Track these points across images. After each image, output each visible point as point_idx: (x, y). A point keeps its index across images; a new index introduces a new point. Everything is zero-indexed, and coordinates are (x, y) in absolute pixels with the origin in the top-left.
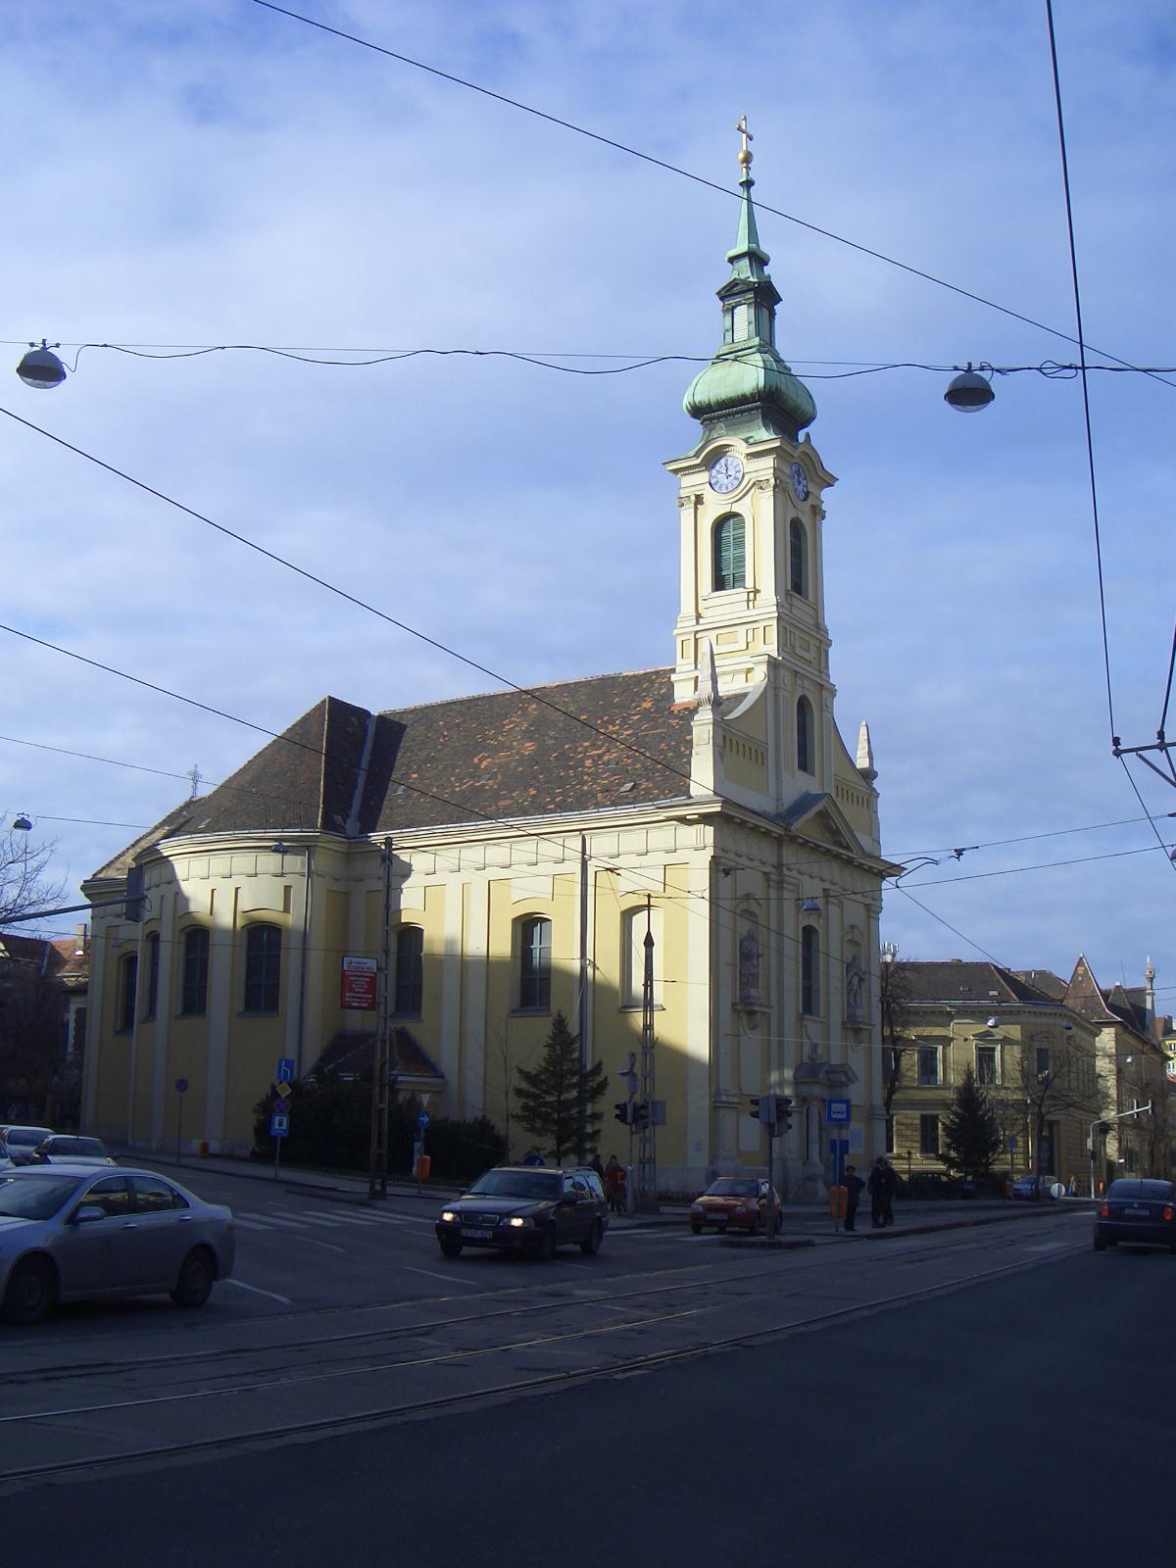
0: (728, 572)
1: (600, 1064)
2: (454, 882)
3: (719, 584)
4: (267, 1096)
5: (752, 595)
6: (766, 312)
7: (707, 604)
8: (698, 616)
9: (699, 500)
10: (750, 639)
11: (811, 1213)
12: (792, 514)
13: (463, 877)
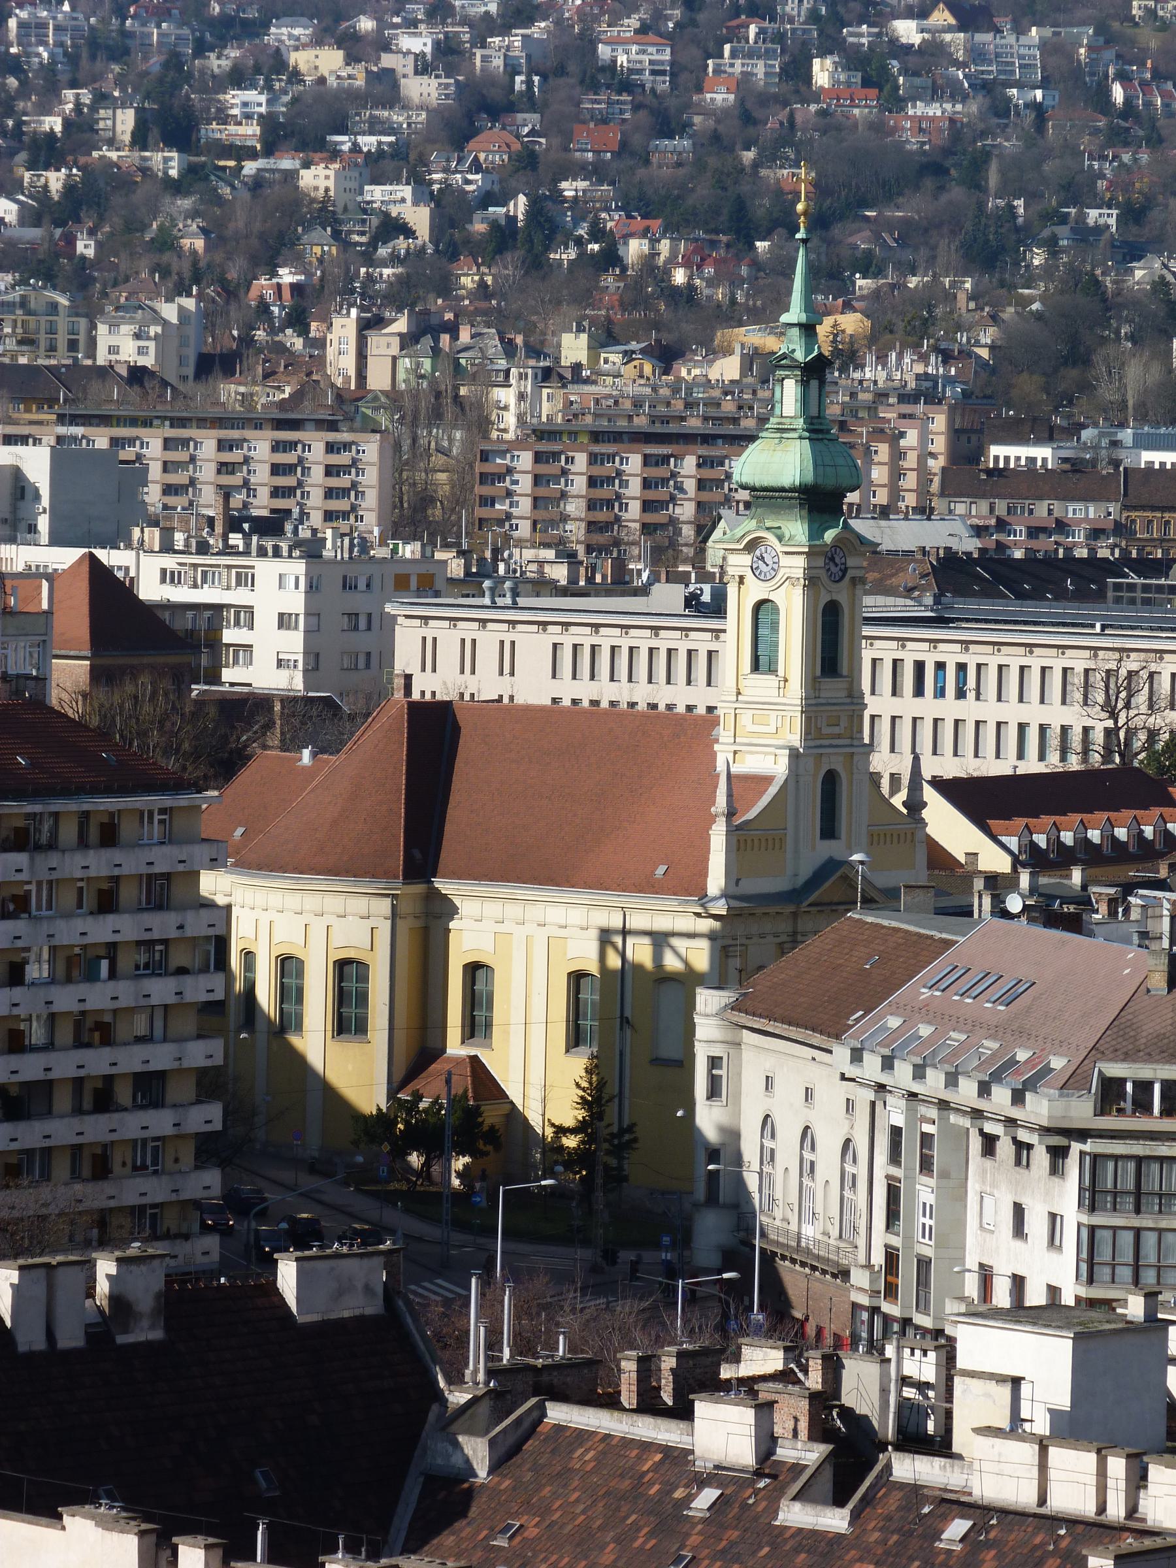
0: (763, 660)
1: (634, 1125)
2: (541, 936)
3: (756, 667)
4: (379, 1109)
5: (782, 683)
6: (814, 384)
7: (746, 683)
8: (739, 693)
9: (741, 580)
10: (779, 725)
11: (184, 427)
12: (824, 599)
13: (530, 928)
